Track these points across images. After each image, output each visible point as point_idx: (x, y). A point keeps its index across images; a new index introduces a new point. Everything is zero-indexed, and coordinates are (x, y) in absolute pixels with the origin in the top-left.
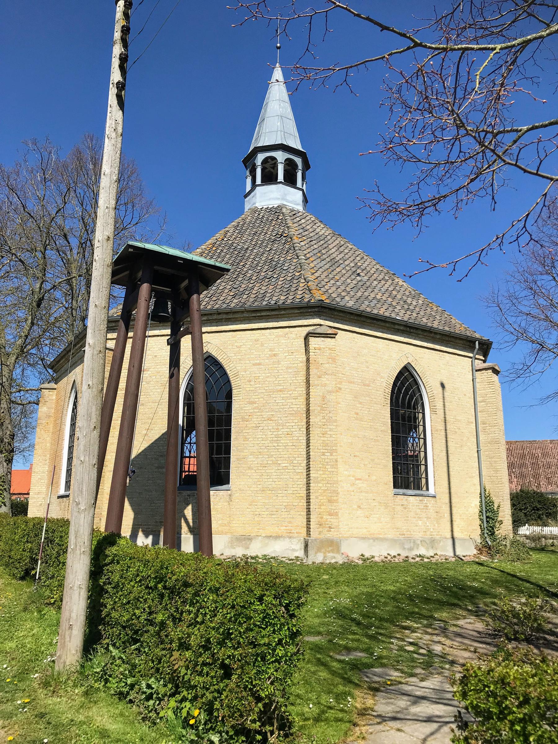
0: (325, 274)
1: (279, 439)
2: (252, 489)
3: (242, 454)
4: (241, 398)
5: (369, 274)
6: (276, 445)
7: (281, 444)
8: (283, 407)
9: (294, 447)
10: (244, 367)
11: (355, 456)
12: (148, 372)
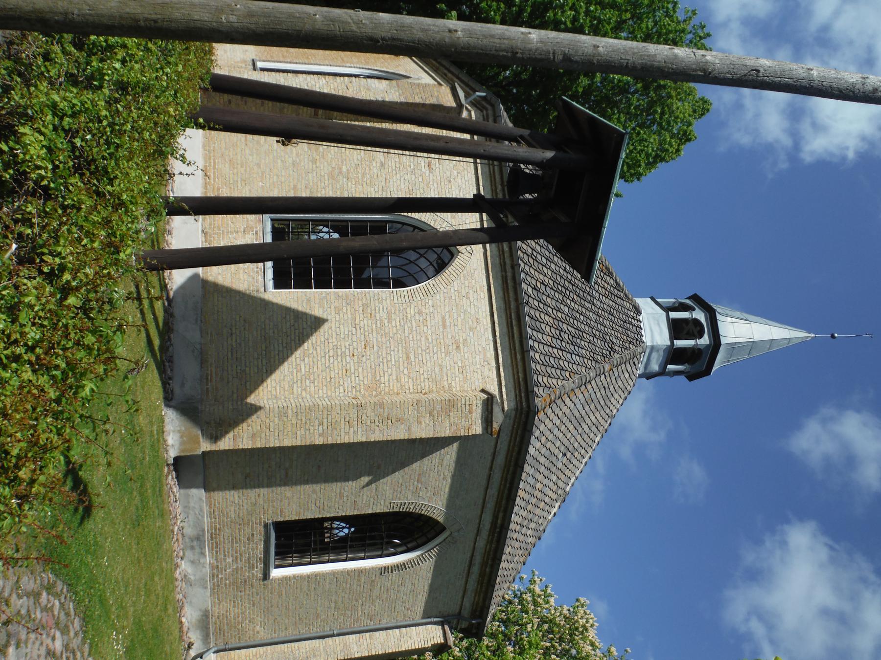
0: (568, 412)
1: (339, 358)
2: (267, 321)
3: (317, 306)
4: (396, 301)
5: (563, 469)
6: (331, 354)
7: (332, 361)
8: (385, 361)
9: (328, 380)
10: (439, 304)
11: (319, 467)
12: (427, 172)
